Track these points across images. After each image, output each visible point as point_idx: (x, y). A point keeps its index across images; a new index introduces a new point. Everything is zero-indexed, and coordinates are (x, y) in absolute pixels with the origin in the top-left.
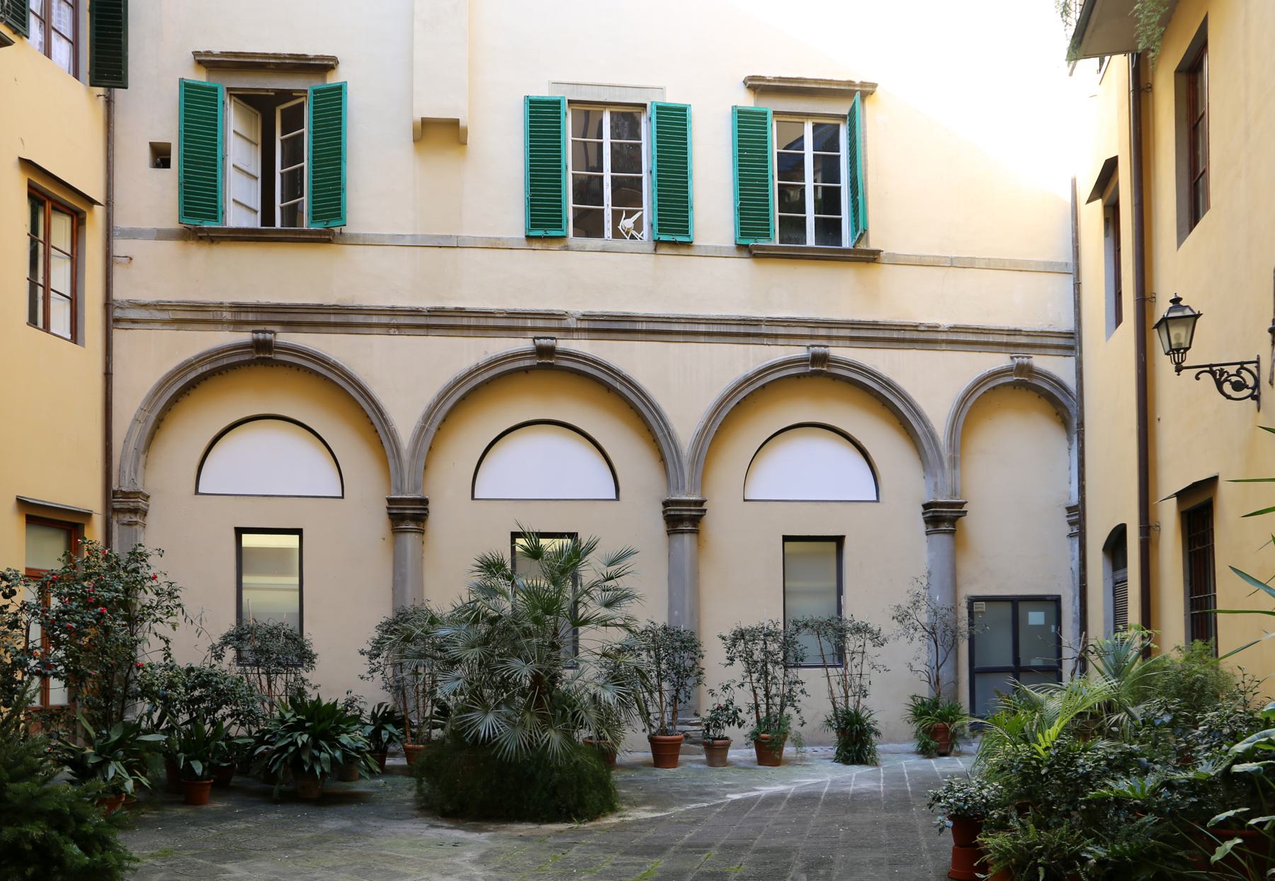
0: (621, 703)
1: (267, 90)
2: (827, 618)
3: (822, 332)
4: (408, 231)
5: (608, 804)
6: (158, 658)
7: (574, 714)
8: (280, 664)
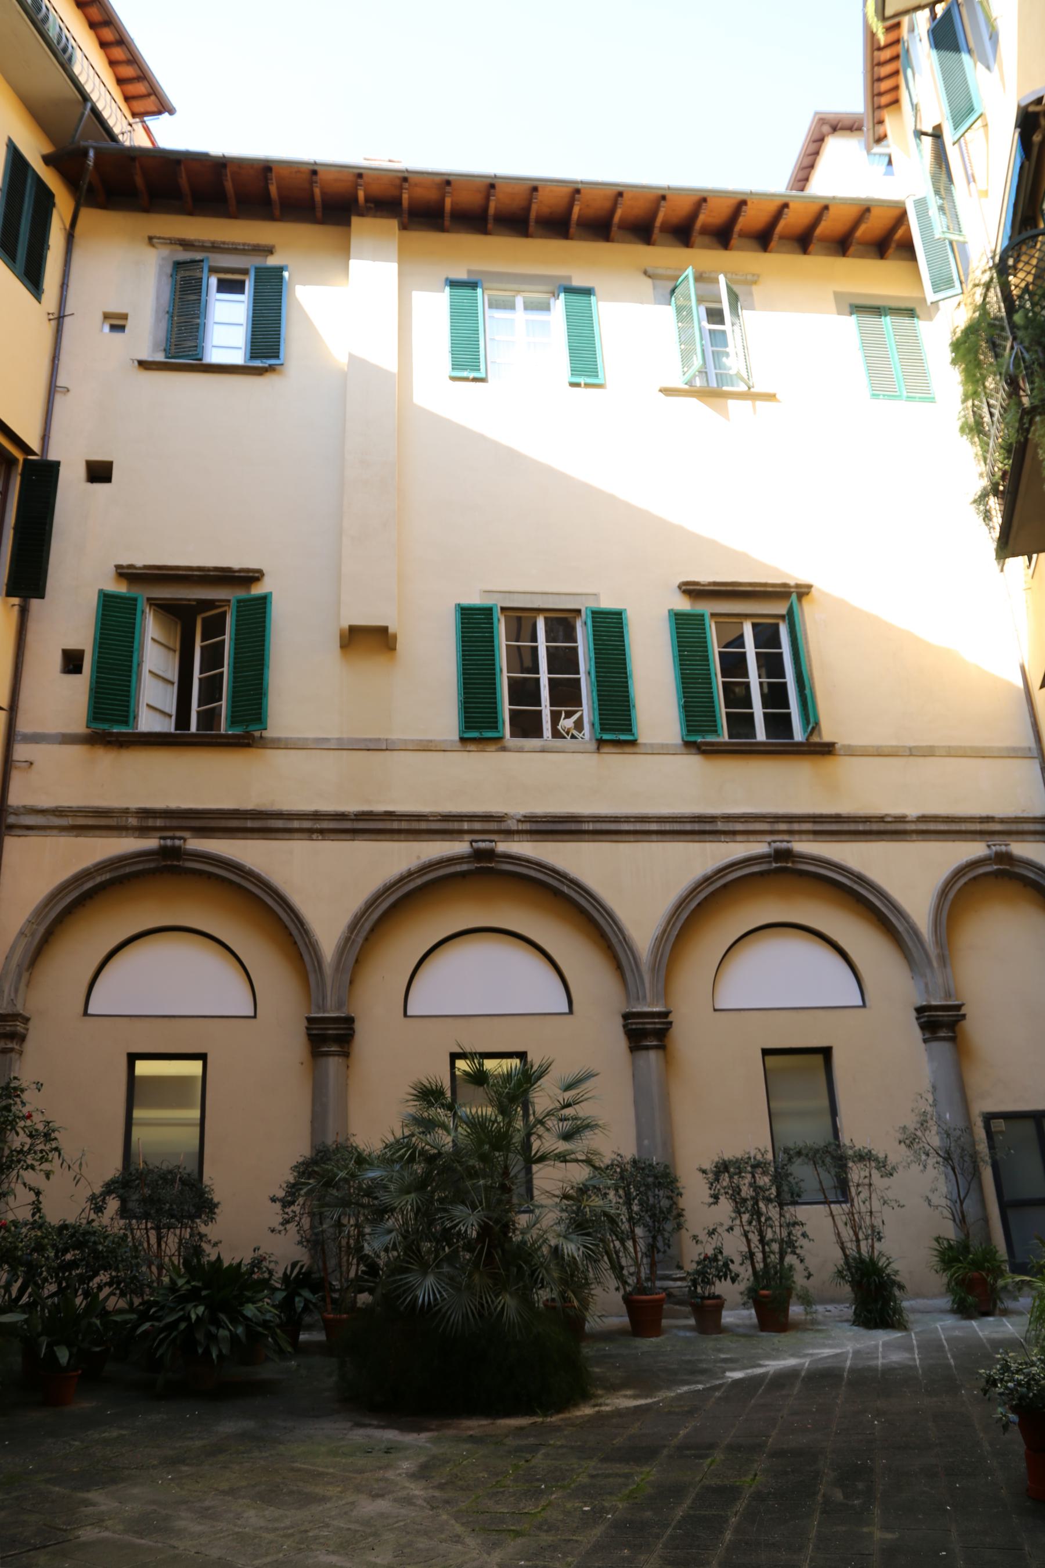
0: (588, 1257)
1: (189, 600)
2: (822, 1144)
3: (783, 827)
4: (334, 735)
5: (580, 1393)
6: (24, 1214)
7: (533, 1272)
8: (172, 1216)
